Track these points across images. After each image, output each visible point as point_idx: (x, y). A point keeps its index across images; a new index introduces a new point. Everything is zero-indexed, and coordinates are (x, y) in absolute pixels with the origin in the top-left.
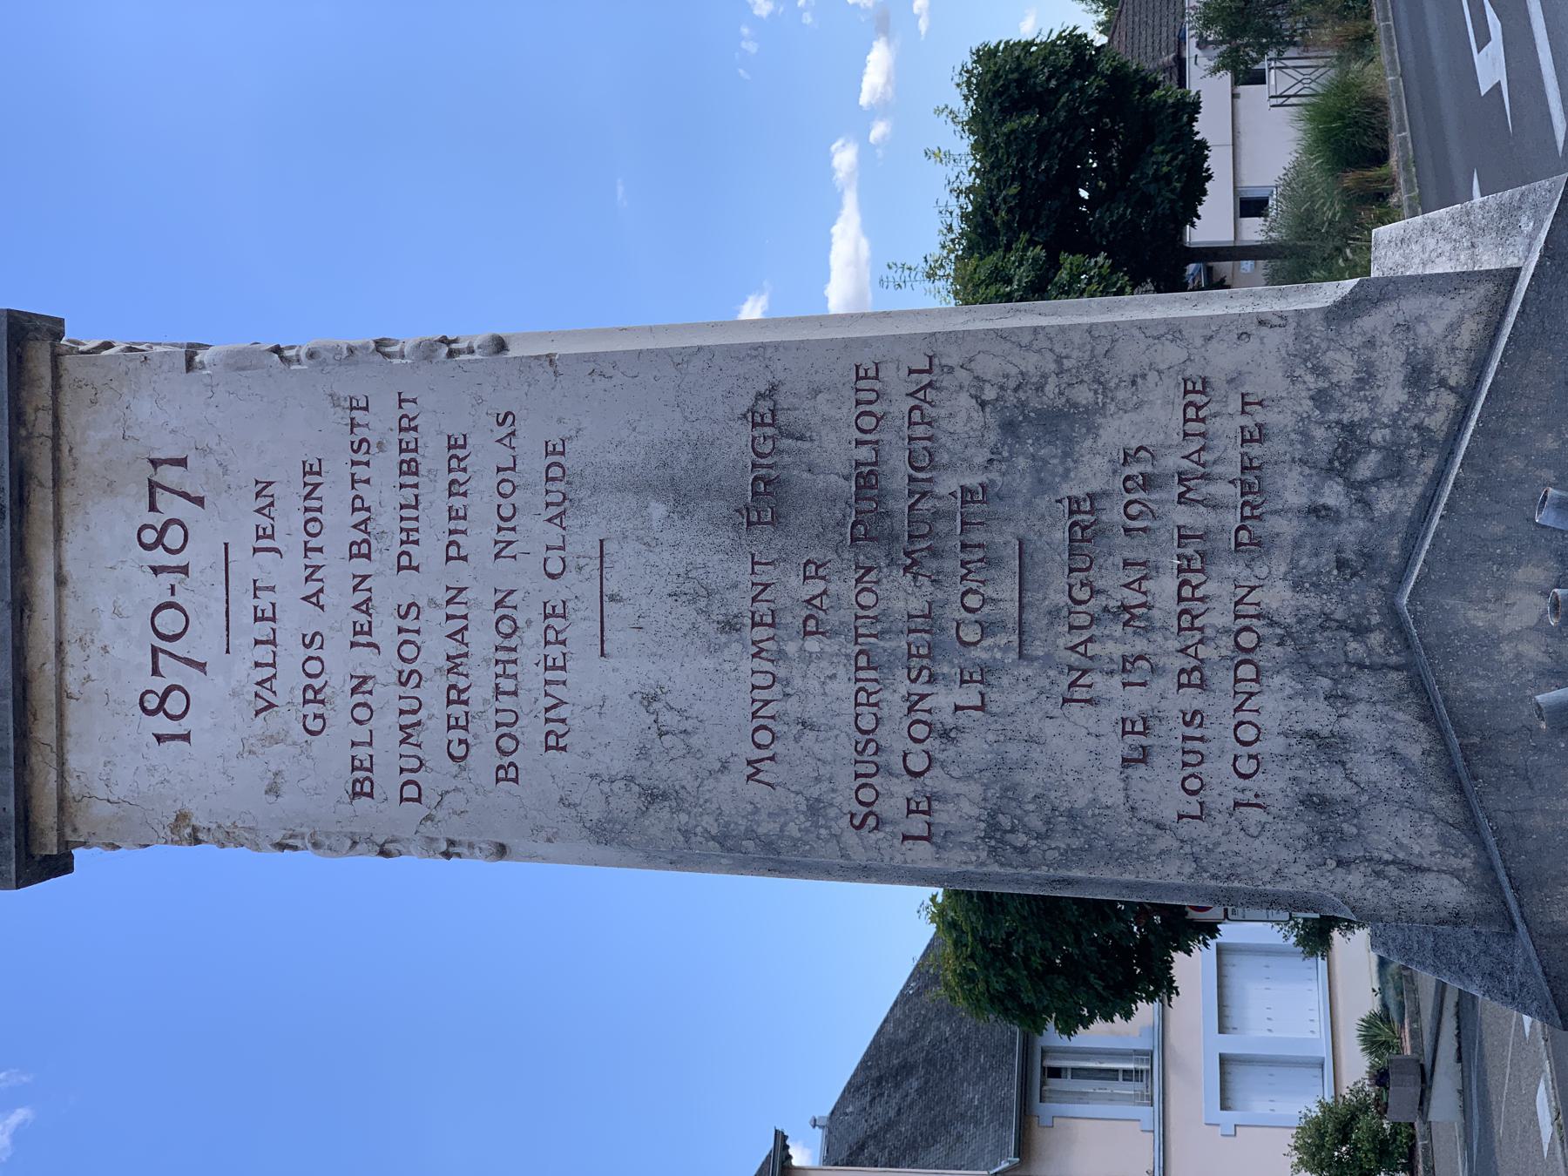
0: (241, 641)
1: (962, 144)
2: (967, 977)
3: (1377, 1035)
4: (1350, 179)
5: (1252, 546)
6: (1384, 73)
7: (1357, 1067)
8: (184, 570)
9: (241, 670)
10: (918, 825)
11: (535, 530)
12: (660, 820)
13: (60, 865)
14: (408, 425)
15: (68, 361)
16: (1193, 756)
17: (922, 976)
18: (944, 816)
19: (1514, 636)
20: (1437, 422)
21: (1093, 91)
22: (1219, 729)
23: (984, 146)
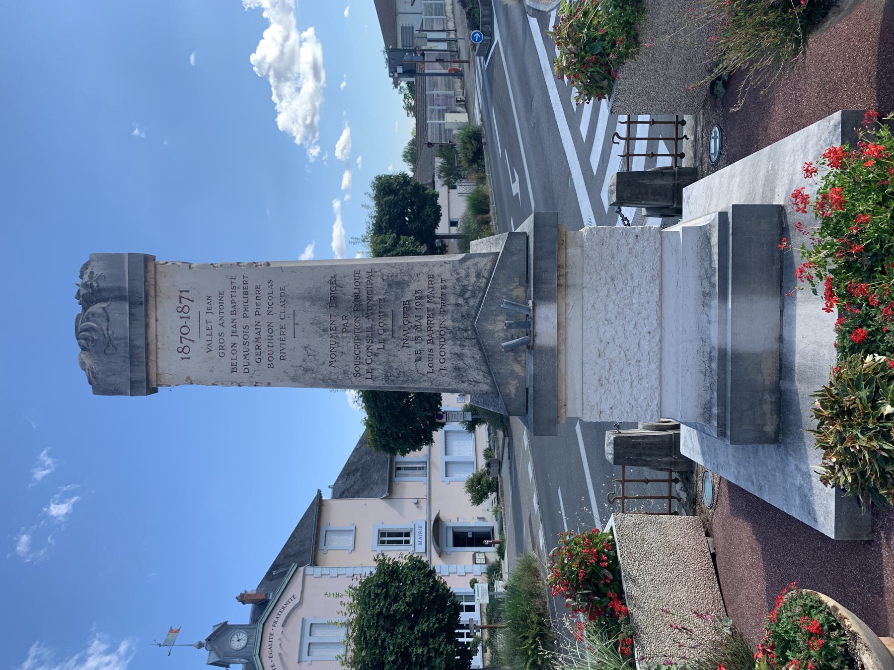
0: (203, 335)
1: (372, 203)
2: (375, 440)
3: (488, 454)
4: (479, 217)
5: (443, 312)
6: (488, 188)
7: (482, 462)
8: (188, 318)
9: (204, 343)
10: (369, 376)
11: (277, 308)
12: (308, 376)
13: (155, 391)
14: (245, 283)
15: (158, 266)
16: (431, 359)
17: (362, 442)
18: (375, 373)
19: (498, 331)
20: (482, 285)
21: (409, 190)
22: (436, 353)
23: (378, 204)
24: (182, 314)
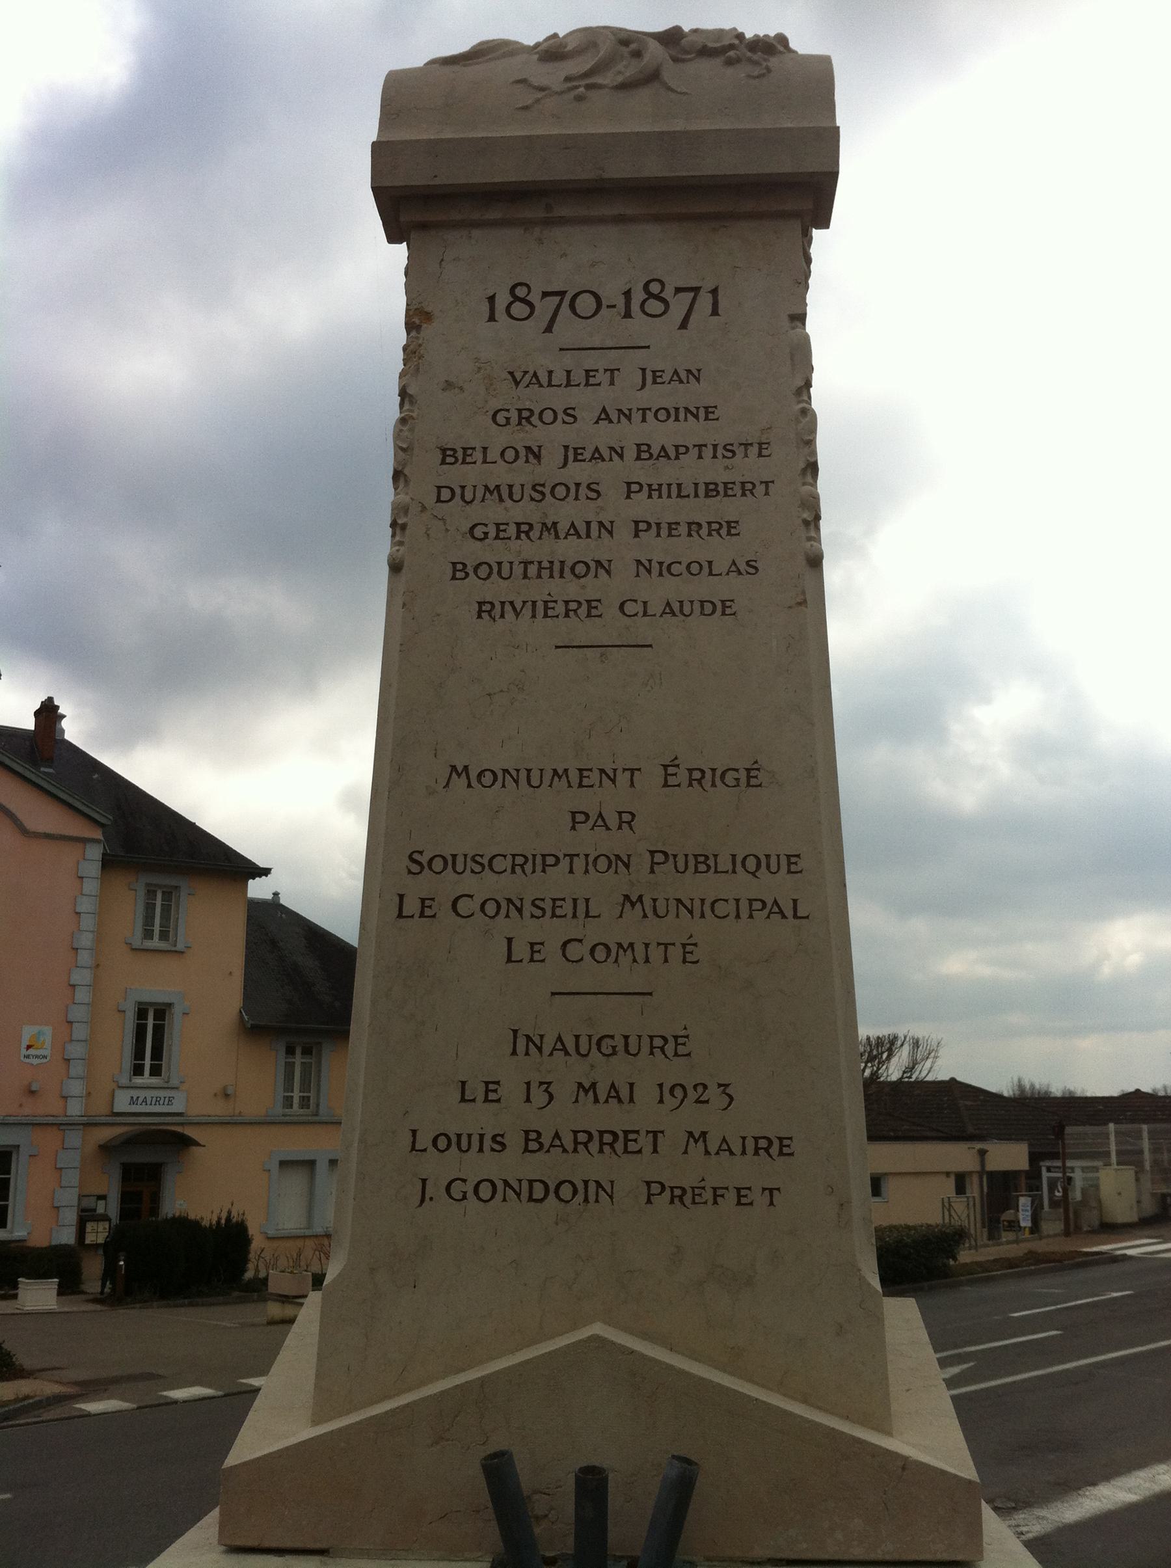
0: (568, 360)
8: (628, 315)
9: (542, 362)
14: (747, 488)
24: (638, 296)
